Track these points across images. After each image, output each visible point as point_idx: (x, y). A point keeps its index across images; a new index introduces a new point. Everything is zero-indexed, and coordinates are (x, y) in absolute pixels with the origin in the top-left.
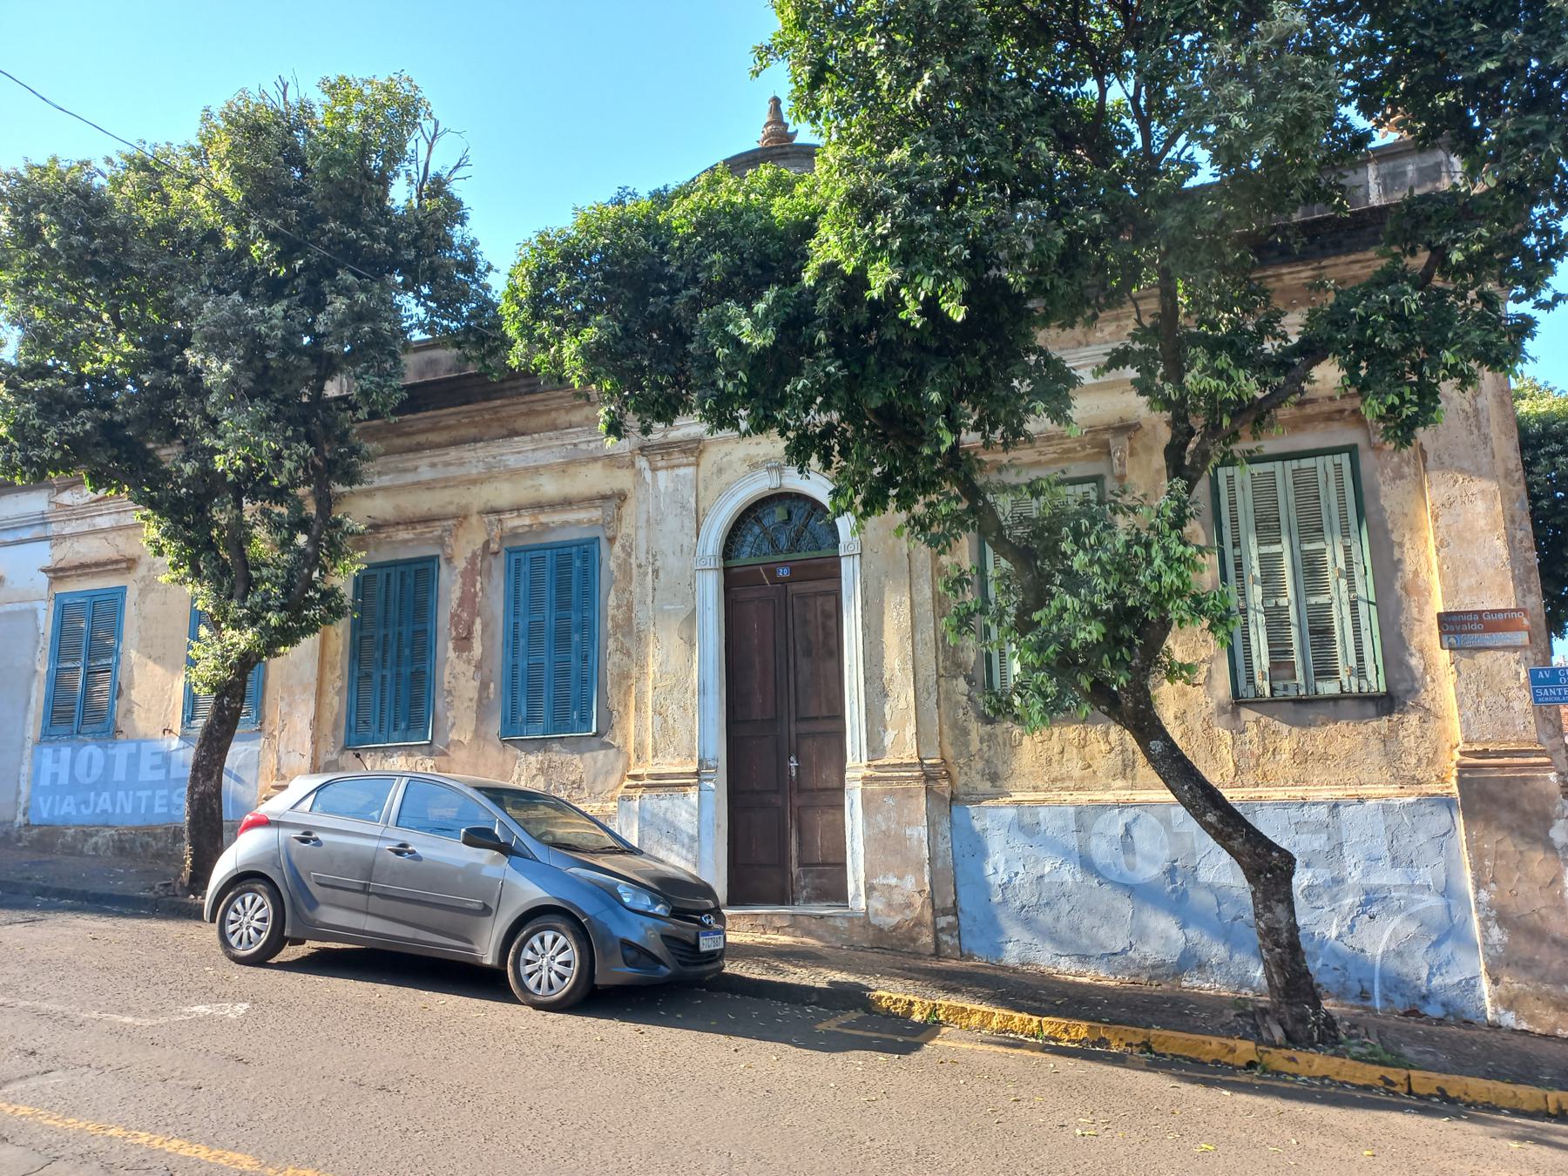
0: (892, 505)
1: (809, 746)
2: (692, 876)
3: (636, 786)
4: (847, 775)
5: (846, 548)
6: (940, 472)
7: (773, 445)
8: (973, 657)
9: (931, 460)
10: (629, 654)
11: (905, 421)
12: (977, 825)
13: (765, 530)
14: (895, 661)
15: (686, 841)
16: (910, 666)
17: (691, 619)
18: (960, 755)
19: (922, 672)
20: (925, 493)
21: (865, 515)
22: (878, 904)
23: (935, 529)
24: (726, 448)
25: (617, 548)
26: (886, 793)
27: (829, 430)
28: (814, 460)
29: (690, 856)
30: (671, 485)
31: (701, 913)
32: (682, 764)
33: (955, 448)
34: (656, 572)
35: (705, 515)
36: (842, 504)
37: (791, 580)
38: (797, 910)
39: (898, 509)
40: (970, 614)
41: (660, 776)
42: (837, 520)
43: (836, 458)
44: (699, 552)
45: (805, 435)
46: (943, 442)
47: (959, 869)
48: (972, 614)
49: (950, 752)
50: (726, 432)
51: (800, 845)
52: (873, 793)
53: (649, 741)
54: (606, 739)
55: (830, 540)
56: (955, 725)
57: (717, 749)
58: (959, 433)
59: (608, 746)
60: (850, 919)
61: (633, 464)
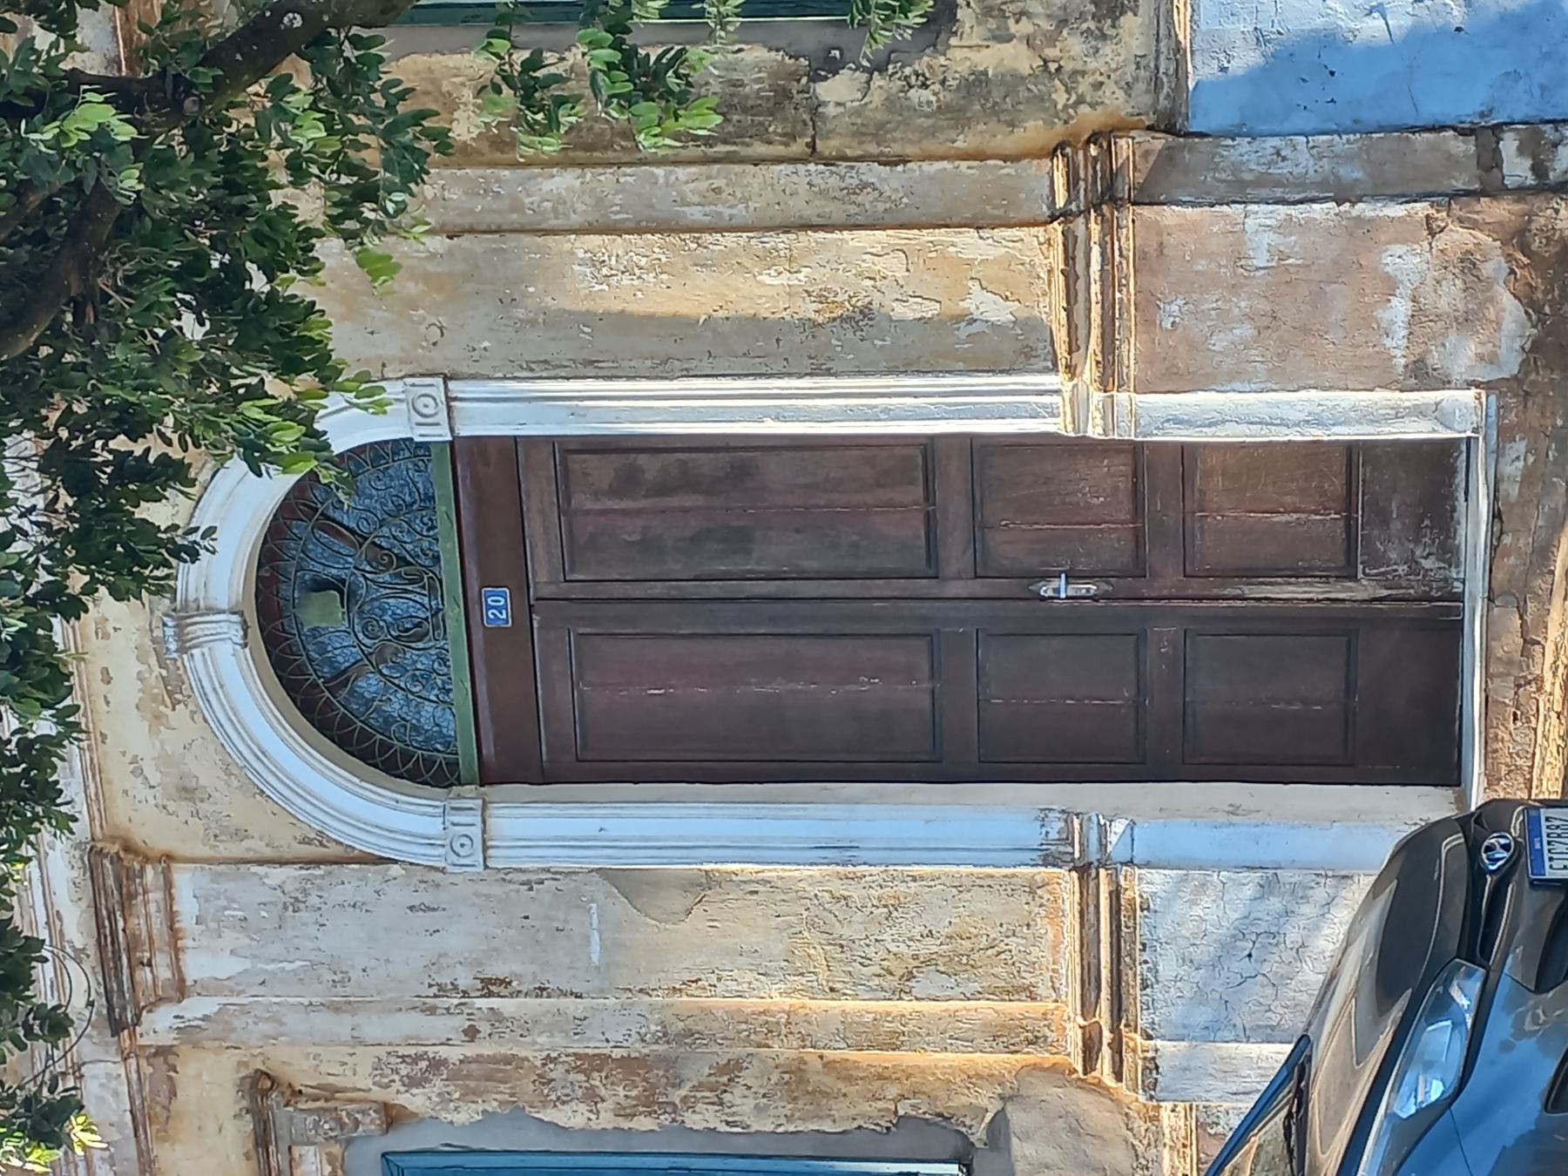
0: (297, 287)
1: (1011, 544)
2: (1375, 890)
3: (1117, 1048)
4: (1094, 432)
5: (426, 420)
6: (198, 142)
7: (109, 639)
8: (756, 54)
9: (156, 165)
10: (732, 1069)
11: (41, 239)
12: (1245, 59)
13: (374, 660)
14: (769, 284)
15: (1275, 904)
16: (781, 241)
17: (629, 884)
18: (1042, 101)
19: (799, 207)
20: (262, 185)
21: (328, 377)
22: (1463, 354)
23: (372, 157)
24: (118, 773)
25: (415, 1101)
26: (1148, 323)
27: (65, 465)
28: (157, 513)
29: (1320, 894)
30: (230, 938)
31: (1477, 874)
32: (1056, 915)
33: (122, 95)
34: (489, 986)
35: (322, 838)
36: (289, 435)
37: (521, 586)
38: (1475, 586)
39: (310, 267)
40: (629, 60)
41: (1089, 979)
42: (339, 446)
43: (151, 447)
44: (434, 856)
45: (80, 540)
46: (103, 130)
47: (1370, 116)
48: (629, 55)
49: (1033, 131)
50: (69, 777)
51: (1295, 575)
52: (1147, 360)
53: (987, 1009)
54: (978, 1134)
55: (402, 466)
56: (954, 115)
57: (1011, 811)
58: (76, 77)
59: (998, 1130)
60: (1505, 434)
61: (163, 1052)
